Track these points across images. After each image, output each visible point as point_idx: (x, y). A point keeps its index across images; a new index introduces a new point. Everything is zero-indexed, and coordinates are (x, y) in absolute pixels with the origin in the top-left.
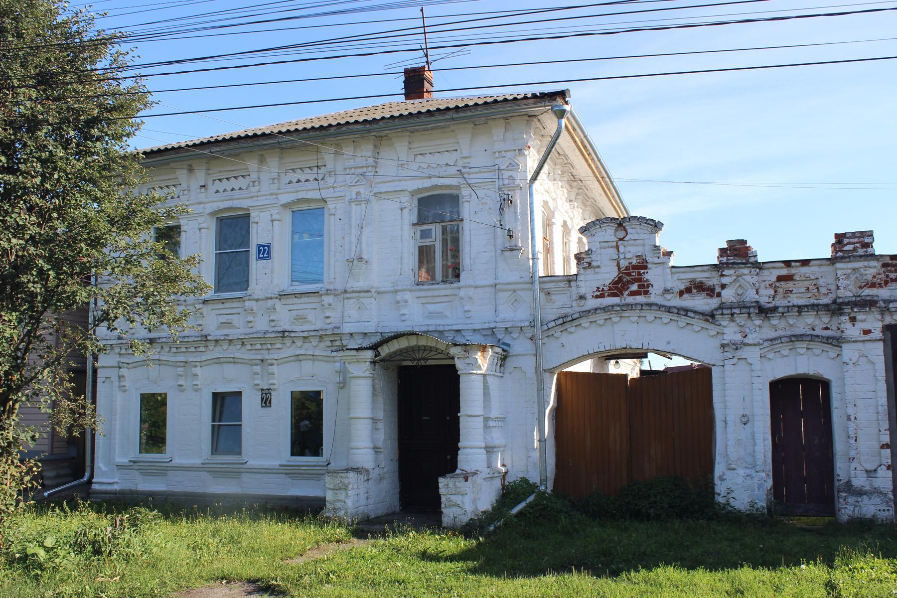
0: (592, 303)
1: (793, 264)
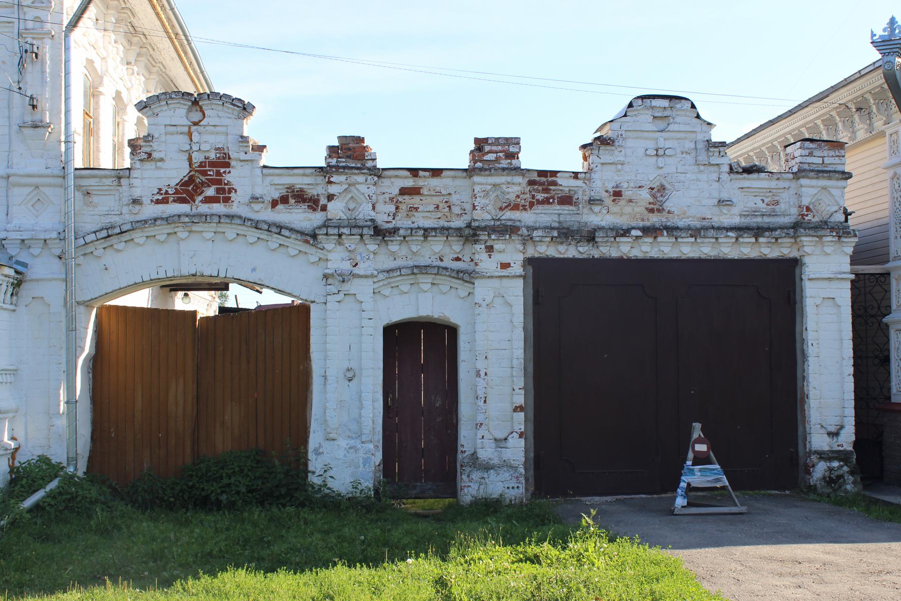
0: (150, 210)
1: (421, 173)
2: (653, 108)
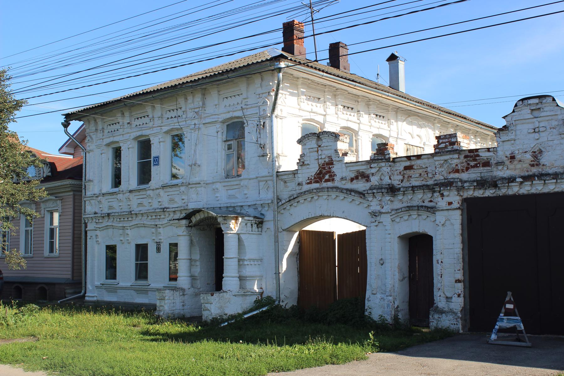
0: (306, 187)
1: (412, 158)
2: (530, 104)
